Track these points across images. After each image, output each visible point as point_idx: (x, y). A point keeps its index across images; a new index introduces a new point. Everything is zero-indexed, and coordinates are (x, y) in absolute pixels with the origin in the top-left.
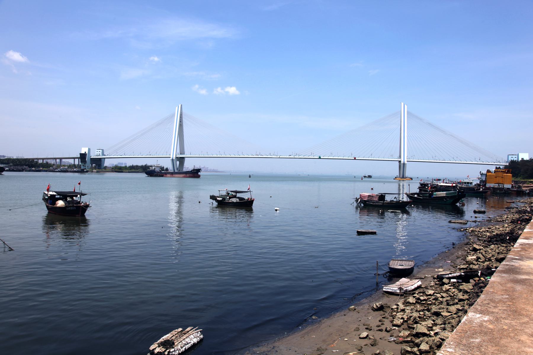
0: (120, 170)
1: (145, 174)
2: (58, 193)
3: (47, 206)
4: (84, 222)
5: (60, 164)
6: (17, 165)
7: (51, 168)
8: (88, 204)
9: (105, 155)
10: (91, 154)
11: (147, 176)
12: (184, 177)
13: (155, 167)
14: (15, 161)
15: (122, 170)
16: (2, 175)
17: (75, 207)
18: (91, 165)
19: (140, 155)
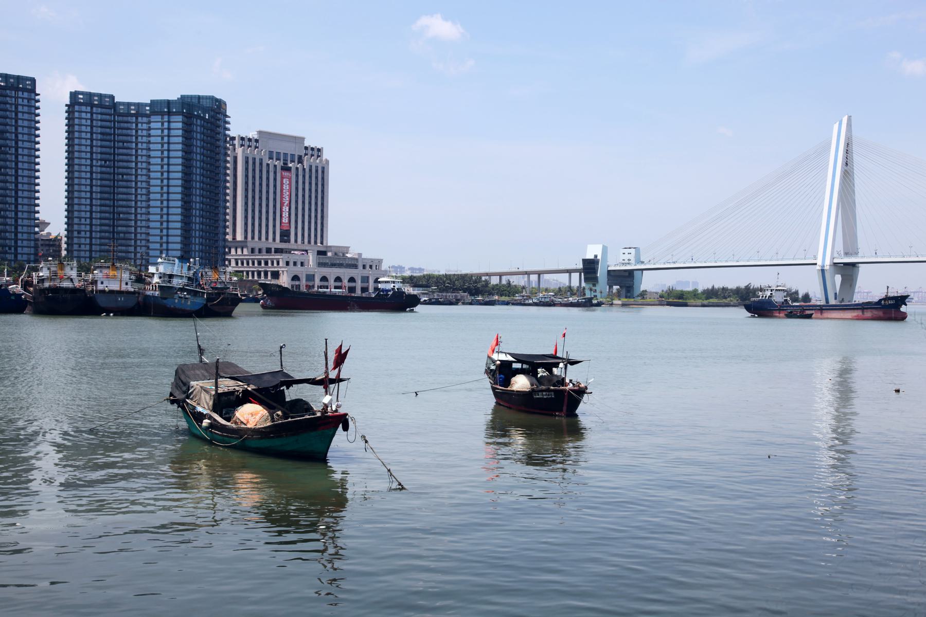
0: (680, 301)
1: (745, 310)
2: (519, 358)
3: (494, 389)
4: (576, 431)
5: (537, 286)
6: (446, 290)
7: (517, 297)
8: (582, 385)
9: (643, 262)
10: (608, 260)
11: (750, 315)
12: (858, 318)
13: (773, 292)
14: (441, 281)
15: (686, 299)
16: (415, 312)
17: (553, 393)
18: (608, 287)
19: (733, 261)
